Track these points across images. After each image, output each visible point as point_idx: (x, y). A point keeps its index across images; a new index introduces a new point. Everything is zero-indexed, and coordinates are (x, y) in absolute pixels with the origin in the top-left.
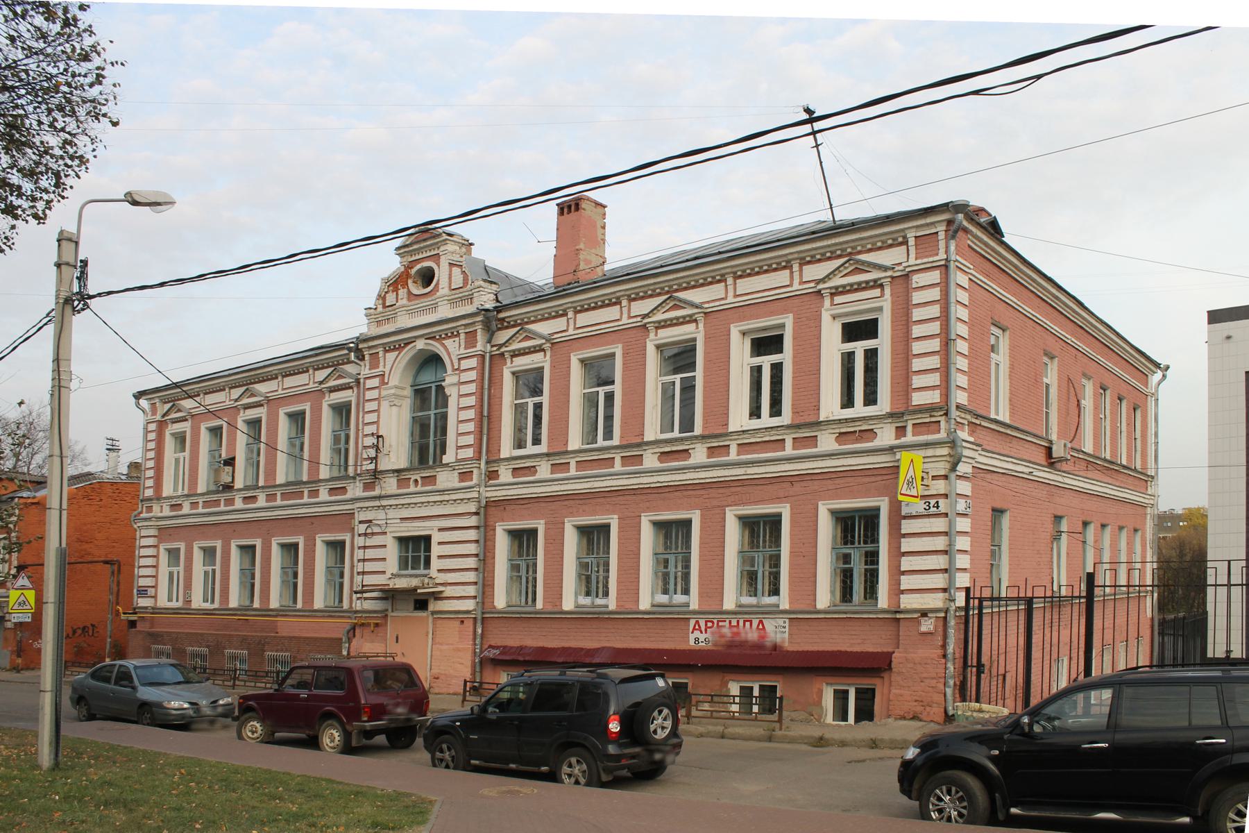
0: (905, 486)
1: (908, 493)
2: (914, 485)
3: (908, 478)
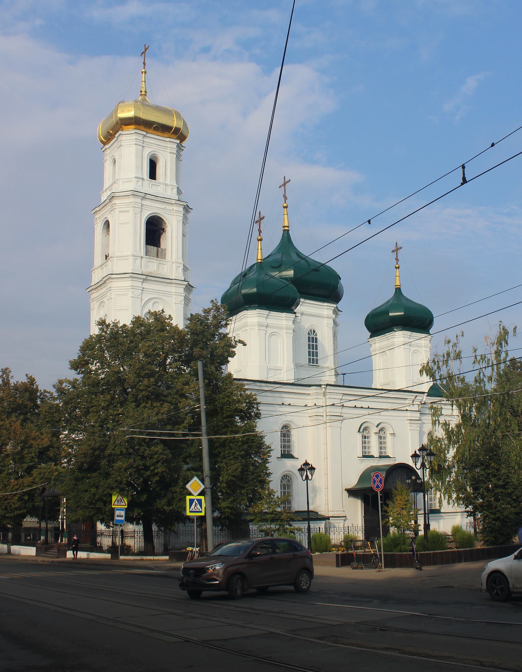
1: (118, 504)
2: (123, 501)
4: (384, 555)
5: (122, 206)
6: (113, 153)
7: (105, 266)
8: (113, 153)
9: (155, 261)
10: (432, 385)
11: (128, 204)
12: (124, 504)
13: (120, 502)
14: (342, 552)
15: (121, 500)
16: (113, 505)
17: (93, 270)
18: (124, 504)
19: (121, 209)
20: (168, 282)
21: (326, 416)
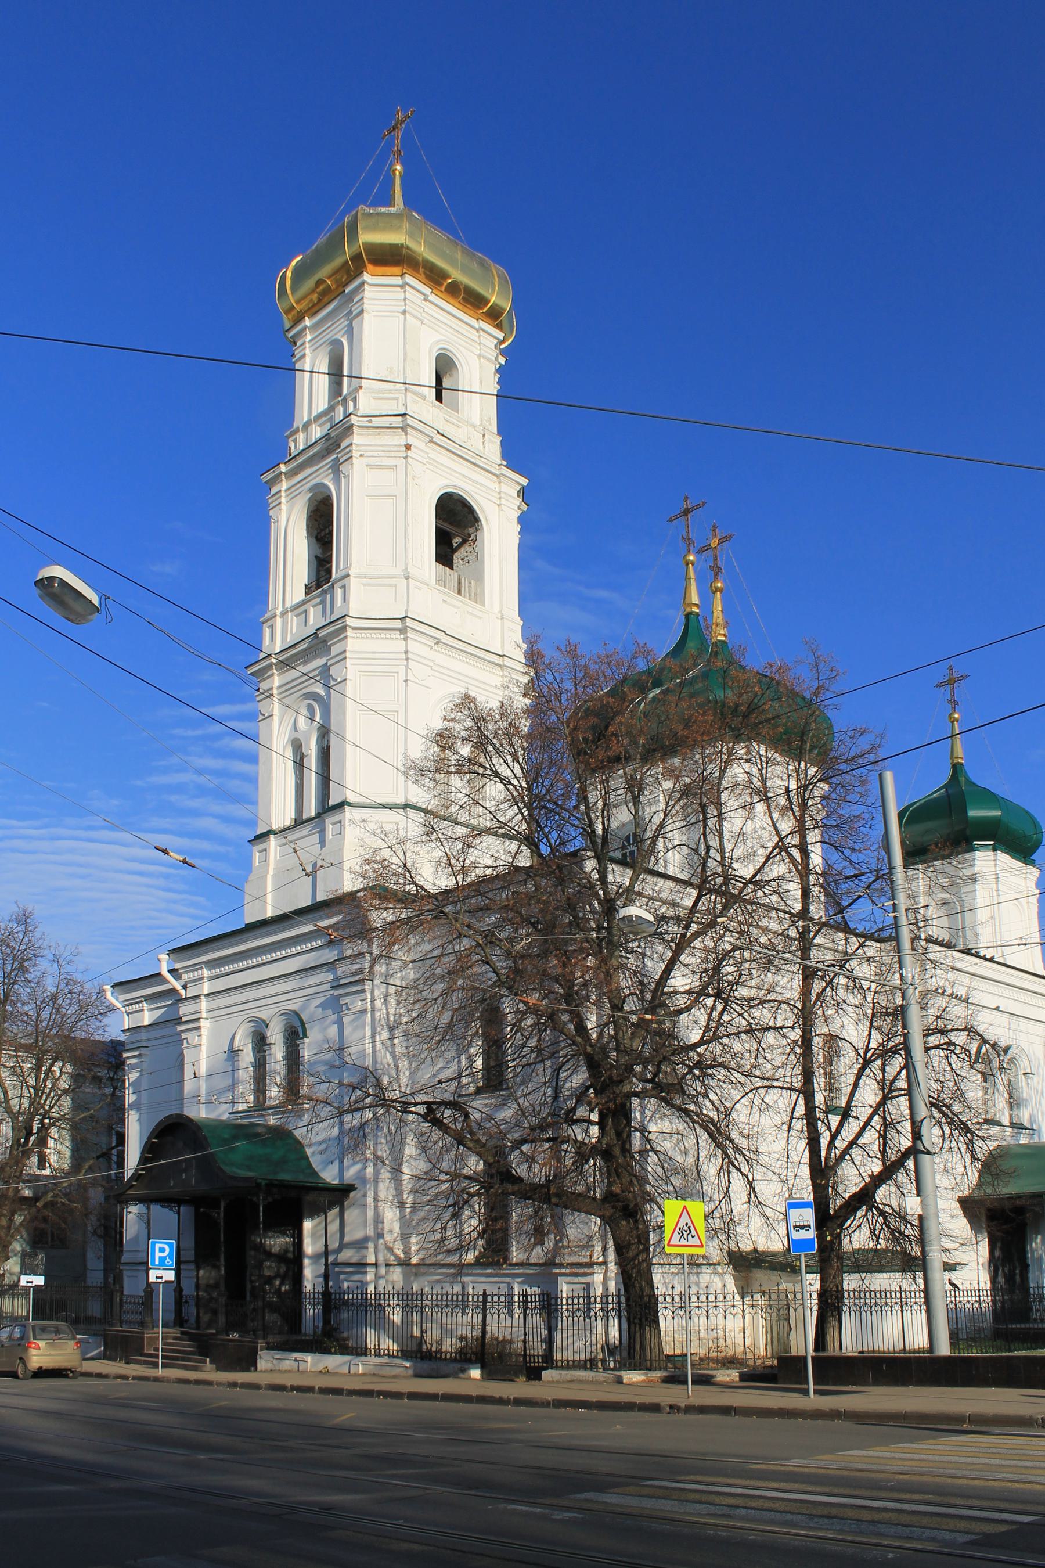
0: (676, 1236)
1: (683, 1242)
2: (694, 1233)
3: (680, 1225)
4: (807, 1383)
5: (375, 454)
6: (334, 332)
7: (313, 606)
8: (334, 332)
9: (459, 604)
10: (697, 1041)
11: (392, 449)
12: (695, 1241)
13: (685, 1234)
14: (253, 1288)
15: (689, 1227)
16: (669, 1245)
17: (267, 620)
18: (695, 1241)
19: (372, 461)
20: (491, 660)
21: (927, 1050)
